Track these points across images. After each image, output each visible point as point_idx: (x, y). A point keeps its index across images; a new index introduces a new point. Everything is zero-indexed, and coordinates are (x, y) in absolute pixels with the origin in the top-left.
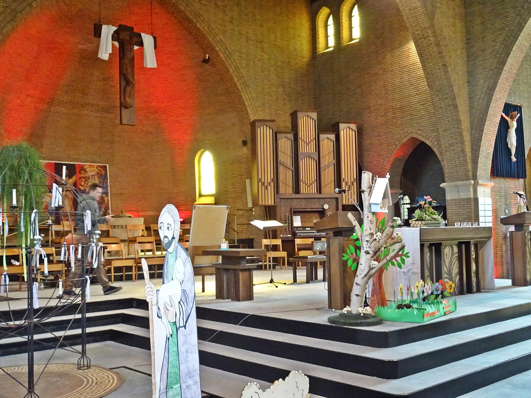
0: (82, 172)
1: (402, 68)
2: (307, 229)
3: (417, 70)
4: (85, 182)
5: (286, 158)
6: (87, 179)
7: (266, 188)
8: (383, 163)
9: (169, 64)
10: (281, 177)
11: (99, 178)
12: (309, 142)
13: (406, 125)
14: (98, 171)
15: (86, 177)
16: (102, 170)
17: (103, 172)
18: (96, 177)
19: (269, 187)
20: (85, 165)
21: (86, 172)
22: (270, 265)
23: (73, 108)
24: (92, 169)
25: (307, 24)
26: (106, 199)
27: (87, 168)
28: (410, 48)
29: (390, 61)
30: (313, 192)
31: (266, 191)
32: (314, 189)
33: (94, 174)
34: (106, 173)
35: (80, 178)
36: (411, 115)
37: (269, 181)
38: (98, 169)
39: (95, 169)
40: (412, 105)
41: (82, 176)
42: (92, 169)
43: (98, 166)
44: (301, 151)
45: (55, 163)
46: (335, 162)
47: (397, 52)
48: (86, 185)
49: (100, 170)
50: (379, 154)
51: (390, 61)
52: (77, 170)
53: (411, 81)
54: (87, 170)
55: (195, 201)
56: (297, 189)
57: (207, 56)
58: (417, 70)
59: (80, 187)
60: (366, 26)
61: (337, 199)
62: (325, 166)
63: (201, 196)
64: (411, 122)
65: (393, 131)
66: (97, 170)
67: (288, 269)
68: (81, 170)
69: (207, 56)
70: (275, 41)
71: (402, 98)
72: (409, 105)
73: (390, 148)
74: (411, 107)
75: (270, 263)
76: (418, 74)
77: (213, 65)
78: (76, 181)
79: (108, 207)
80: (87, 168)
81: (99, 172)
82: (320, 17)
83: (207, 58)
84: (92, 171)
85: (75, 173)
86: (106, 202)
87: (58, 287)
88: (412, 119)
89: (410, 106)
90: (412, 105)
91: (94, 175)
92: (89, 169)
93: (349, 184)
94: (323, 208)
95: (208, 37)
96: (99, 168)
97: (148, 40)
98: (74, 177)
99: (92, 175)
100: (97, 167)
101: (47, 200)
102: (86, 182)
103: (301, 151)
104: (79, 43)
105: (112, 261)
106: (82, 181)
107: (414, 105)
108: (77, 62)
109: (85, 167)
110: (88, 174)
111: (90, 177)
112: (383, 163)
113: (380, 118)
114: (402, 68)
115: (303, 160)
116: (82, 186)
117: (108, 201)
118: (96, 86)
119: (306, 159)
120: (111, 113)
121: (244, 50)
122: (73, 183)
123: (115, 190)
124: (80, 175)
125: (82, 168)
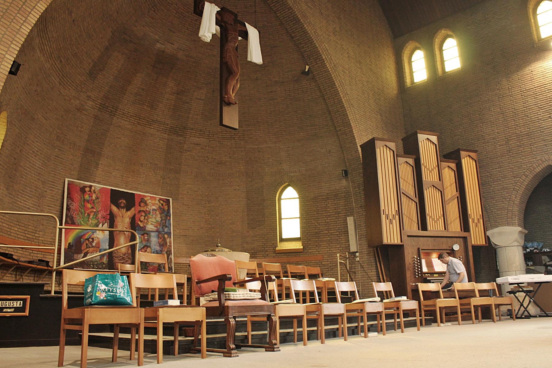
0: (142, 204)
1: (525, 92)
2: (435, 275)
3: (547, 92)
4: (145, 217)
5: (409, 187)
6: (147, 213)
7: (391, 222)
8: (509, 197)
9: (257, 80)
10: (405, 211)
11: (161, 214)
12: (432, 170)
13: (538, 152)
14: (161, 205)
15: (146, 211)
16: (164, 204)
17: (166, 208)
18: (158, 212)
19: (394, 221)
20: (146, 196)
21: (146, 204)
22: (421, 320)
23: (138, 123)
24: (154, 202)
25: (393, 58)
26: (168, 240)
27: (148, 200)
28: (533, 70)
29: (507, 86)
30: (441, 229)
31: (391, 225)
32: (440, 225)
33: (155, 208)
34: (169, 209)
35: (140, 212)
36: (544, 140)
37: (394, 213)
38: (160, 202)
39: (157, 202)
40: (544, 130)
41: (142, 209)
42: (154, 202)
43: (160, 199)
44: (425, 179)
45: (111, 189)
46: (458, 194)
47: (520, 73)
48: (146, 221)
49: (162, 205)
50: (503, 187)
51: (507, 86)
52: (137, 200)
53: (539, 105)
54: (148, 202)
55: (276, 246)
56: (423, 226)
57: (307, 67)
58: (547, 92)
59: (139, 223)
60: (465, 55)
61: (465, 238)
62: (449, 200)
63: (282, 240)
64: (546, 148)
65: (521, 160)
66: (158, 203)
67: (462, 324)
68: (141, 202)
69: (307, 67)
70: (371, 65)
71: (528, 123)
72: (540, 130)
73: (518, 179)
74: (543, 132)
75: (421, 318)
76: (548, 96)
77: (313, 78)
78: (135, 215)
79: (171, 251)
80: (148, 200)
81: (162, 207)
82: (405, 52)
83: (307, 70)
84: (153, 205)
85: (134, 205)
86: (168, 244)
87: (528, 271)
88: (545, 145)
89: (542, 131)
90: (544, 130)
91: (156, 210)
92: (150, 201)
93: (476, 221)
94: (453, 250)
95: (315, 42)
96: (162, 202)
97: (253, 33)
98: (133, 209)
99: (153, 210)
100: (159, 201)
101: (98, 236)
102: (146, 218)
103: (425, 179)
104: (158, 42)
105: (130, 335)
106: (142, 216)
107: (547, 130)
108: (151, 65)
109: (146, 199)
110: (149, 207)
111: (151, 211)
112: (509, 197)
113: (499, 147)
114: (525, 92)
115: (428, 190)
116: (141, 222)
117: (170, 243)
118: (168, 99)
119: (430, 188)
120: (181, 136)
121: (347, 66)
122: (131, 217)
123: (178, 231)
124: (139, 207)
125: (143, 200)
